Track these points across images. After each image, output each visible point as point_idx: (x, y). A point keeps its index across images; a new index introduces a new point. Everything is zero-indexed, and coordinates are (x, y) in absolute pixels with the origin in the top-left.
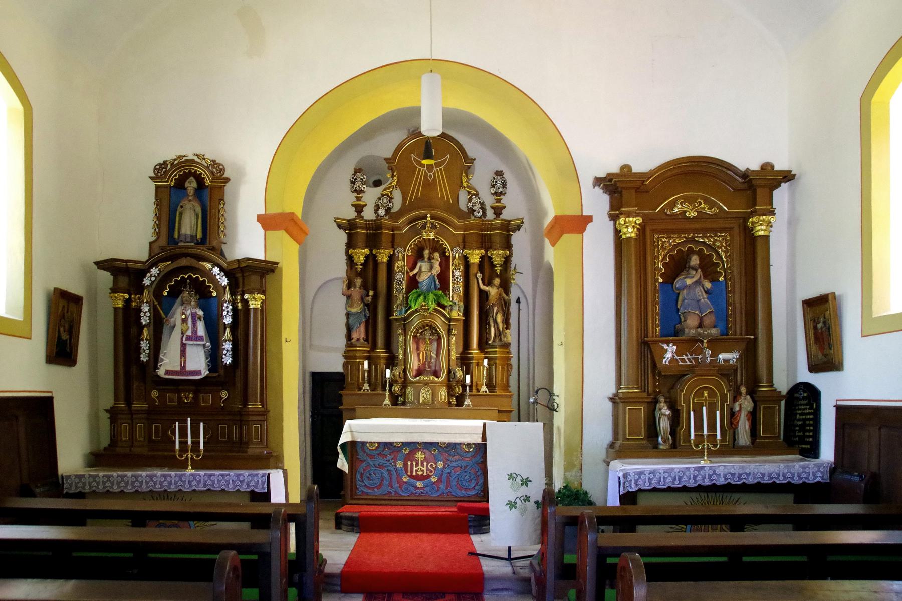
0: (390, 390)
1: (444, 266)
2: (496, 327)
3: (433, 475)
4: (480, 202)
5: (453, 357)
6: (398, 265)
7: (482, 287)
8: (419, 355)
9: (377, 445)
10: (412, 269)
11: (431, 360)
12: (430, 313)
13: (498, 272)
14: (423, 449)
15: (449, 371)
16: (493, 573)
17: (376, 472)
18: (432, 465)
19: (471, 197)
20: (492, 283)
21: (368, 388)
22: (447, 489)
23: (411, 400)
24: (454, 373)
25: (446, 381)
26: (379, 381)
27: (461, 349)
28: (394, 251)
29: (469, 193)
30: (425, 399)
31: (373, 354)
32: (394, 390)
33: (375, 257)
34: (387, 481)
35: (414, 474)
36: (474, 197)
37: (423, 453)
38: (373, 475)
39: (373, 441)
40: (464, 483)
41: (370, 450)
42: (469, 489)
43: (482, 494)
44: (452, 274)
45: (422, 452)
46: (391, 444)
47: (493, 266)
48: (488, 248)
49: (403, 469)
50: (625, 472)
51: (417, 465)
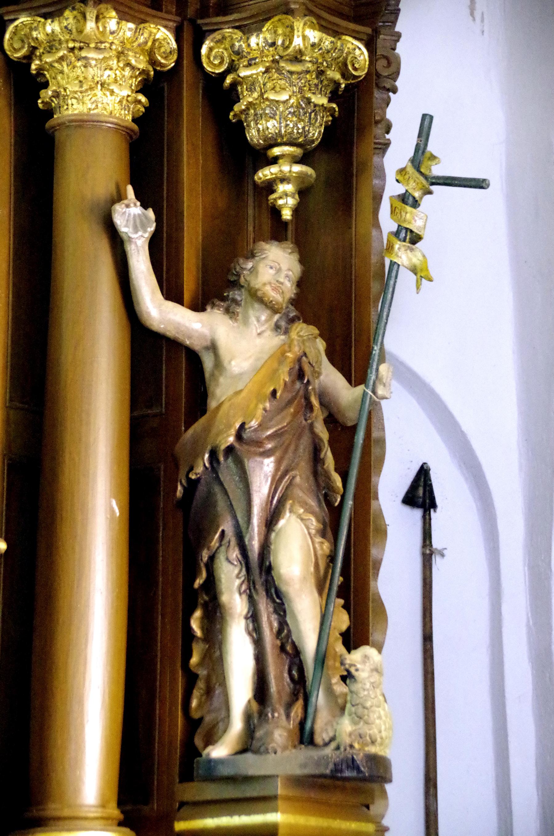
16: (218, 560)
20: (235, 284)
50: (411, 245)
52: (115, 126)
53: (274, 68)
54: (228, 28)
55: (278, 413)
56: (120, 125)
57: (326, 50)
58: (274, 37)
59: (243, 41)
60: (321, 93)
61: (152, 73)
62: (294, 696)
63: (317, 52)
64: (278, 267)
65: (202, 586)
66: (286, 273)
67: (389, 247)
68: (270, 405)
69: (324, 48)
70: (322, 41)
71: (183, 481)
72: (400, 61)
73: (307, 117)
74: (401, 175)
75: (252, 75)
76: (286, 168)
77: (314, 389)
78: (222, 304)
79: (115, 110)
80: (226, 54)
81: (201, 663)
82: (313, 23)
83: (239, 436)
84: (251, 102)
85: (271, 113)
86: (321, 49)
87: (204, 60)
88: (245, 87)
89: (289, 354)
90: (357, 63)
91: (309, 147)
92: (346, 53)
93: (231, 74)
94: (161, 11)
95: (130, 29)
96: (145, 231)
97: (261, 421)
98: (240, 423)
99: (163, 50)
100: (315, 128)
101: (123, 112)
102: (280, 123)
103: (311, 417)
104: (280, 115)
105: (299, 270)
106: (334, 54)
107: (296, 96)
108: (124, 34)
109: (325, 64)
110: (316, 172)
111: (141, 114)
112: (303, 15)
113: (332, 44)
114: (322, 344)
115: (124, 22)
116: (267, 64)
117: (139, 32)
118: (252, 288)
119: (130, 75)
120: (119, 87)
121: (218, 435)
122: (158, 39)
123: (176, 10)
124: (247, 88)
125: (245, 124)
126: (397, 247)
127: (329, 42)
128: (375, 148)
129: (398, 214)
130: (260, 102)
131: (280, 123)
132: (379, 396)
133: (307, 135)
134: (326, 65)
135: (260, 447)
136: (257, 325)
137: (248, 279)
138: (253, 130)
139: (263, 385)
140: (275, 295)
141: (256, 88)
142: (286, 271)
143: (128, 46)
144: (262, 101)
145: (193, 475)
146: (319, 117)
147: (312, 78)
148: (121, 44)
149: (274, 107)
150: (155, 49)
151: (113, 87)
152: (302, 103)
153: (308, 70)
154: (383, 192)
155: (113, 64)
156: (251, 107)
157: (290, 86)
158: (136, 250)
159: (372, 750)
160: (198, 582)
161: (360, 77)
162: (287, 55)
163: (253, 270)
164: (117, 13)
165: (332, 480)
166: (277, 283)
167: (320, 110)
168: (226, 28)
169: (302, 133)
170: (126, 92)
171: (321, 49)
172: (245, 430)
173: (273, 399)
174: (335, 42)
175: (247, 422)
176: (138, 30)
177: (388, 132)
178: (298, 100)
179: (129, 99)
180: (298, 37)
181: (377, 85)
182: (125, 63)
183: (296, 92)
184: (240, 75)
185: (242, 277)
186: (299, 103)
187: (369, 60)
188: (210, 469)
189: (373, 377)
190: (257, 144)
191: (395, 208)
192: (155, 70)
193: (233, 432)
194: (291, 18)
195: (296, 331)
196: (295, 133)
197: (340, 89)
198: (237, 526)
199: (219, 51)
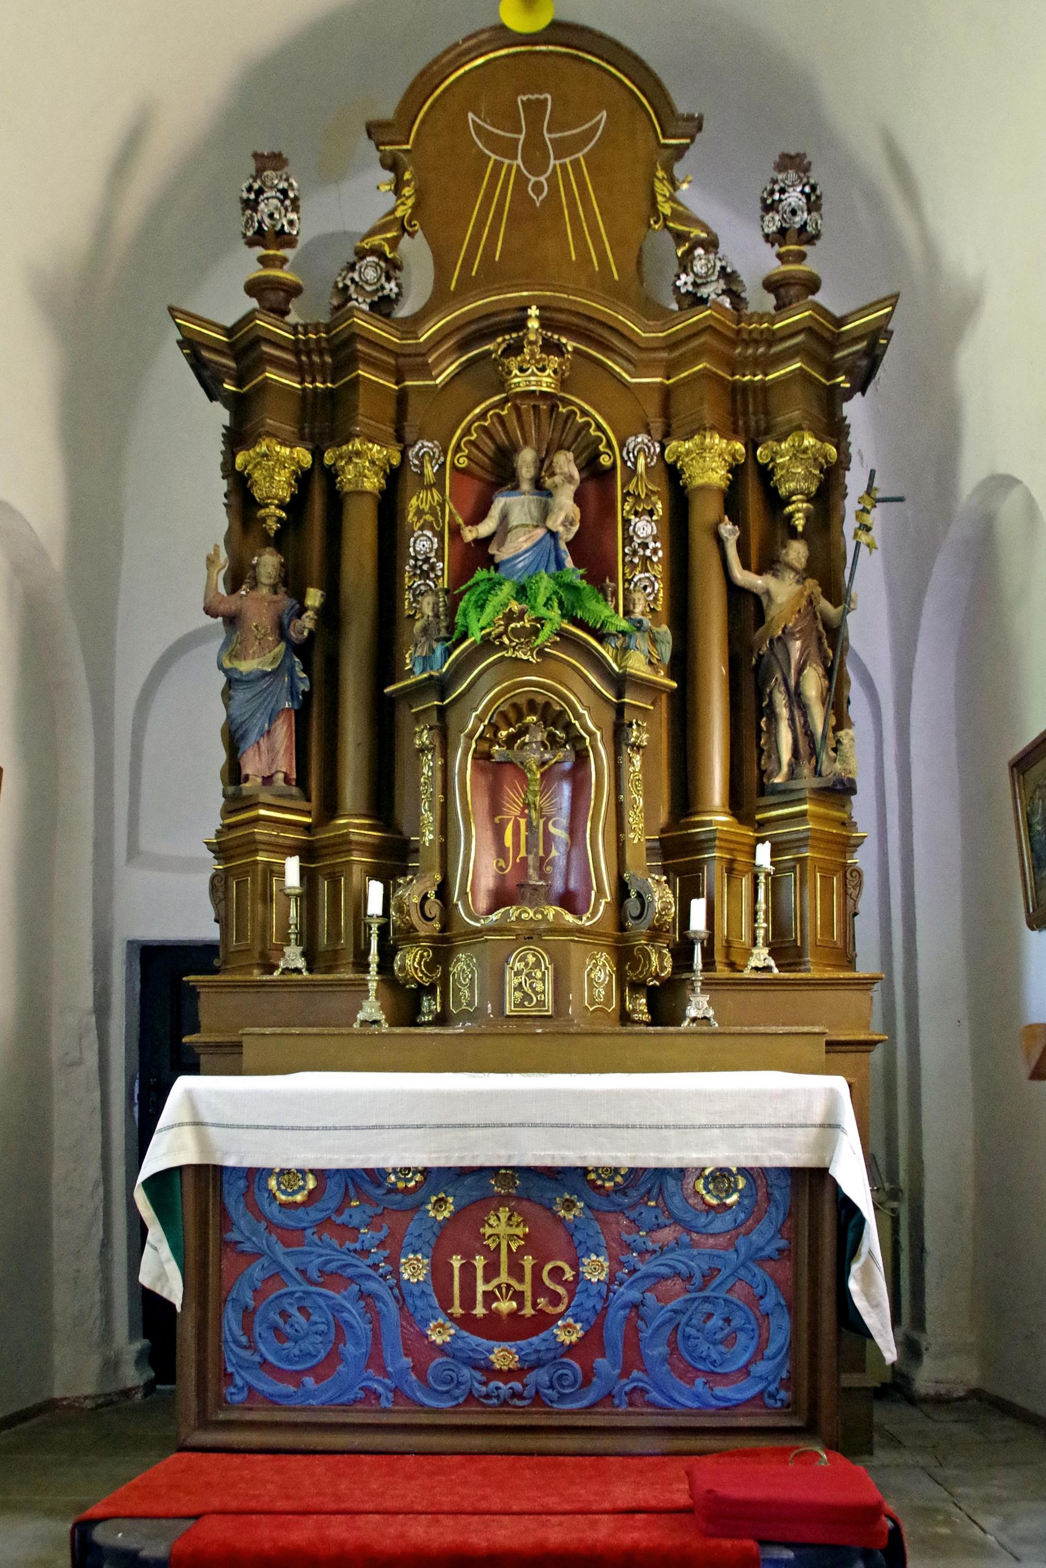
0: (385, 966)
1: (593, 505)
2: (799, 721)
3: (561, 1316)
4: (723, 268)
5: (637, 836)
6: (416, 502)
7: (742, 576)
8: (498, 832)
9: (311, 1184)
10: (479, 516)
11: (547, 851)
12: (541, 653)
13: (800, 523)
14: (518, 1198)
15: (622, 889)
17: (307, 1303)
18: (557, 1273)
19: (690, 252)
20: (778, 561)
21: (301, 963)
22: (625, 1373)
23: (470, 1004)
24: (639, 896)
25: (610, 929)
26: (345, 942)
27: (663, 817)
28: (404, 453)
29: (680, 238)
30: (527, 997)
31: (324, 835)
32: (402, 968)
33: (331, 475)
34: (357, 1344)
35: (479, 1311)
36: (700, 251)
37: (517, 1218)
38: (299, 1318)
39: (292, 1165)
40: (704, 1348)
41: (283, 1205)
42: (725, 1374)
43: (783, 1394)
44: (625, 530)
45: (512, 1210)
46: (376, 1176)
47: (775, 502)
48: (758, 433)
49: (430, 1290)
51: (492, 1271)
62: (811, 755)
65: (767, 706)
81: (765, 744)
83: (783, 632)
147: (811, 461)
159: (851, 776)
160: (764, 704)
170: (723, 472)
198: (783, 674)
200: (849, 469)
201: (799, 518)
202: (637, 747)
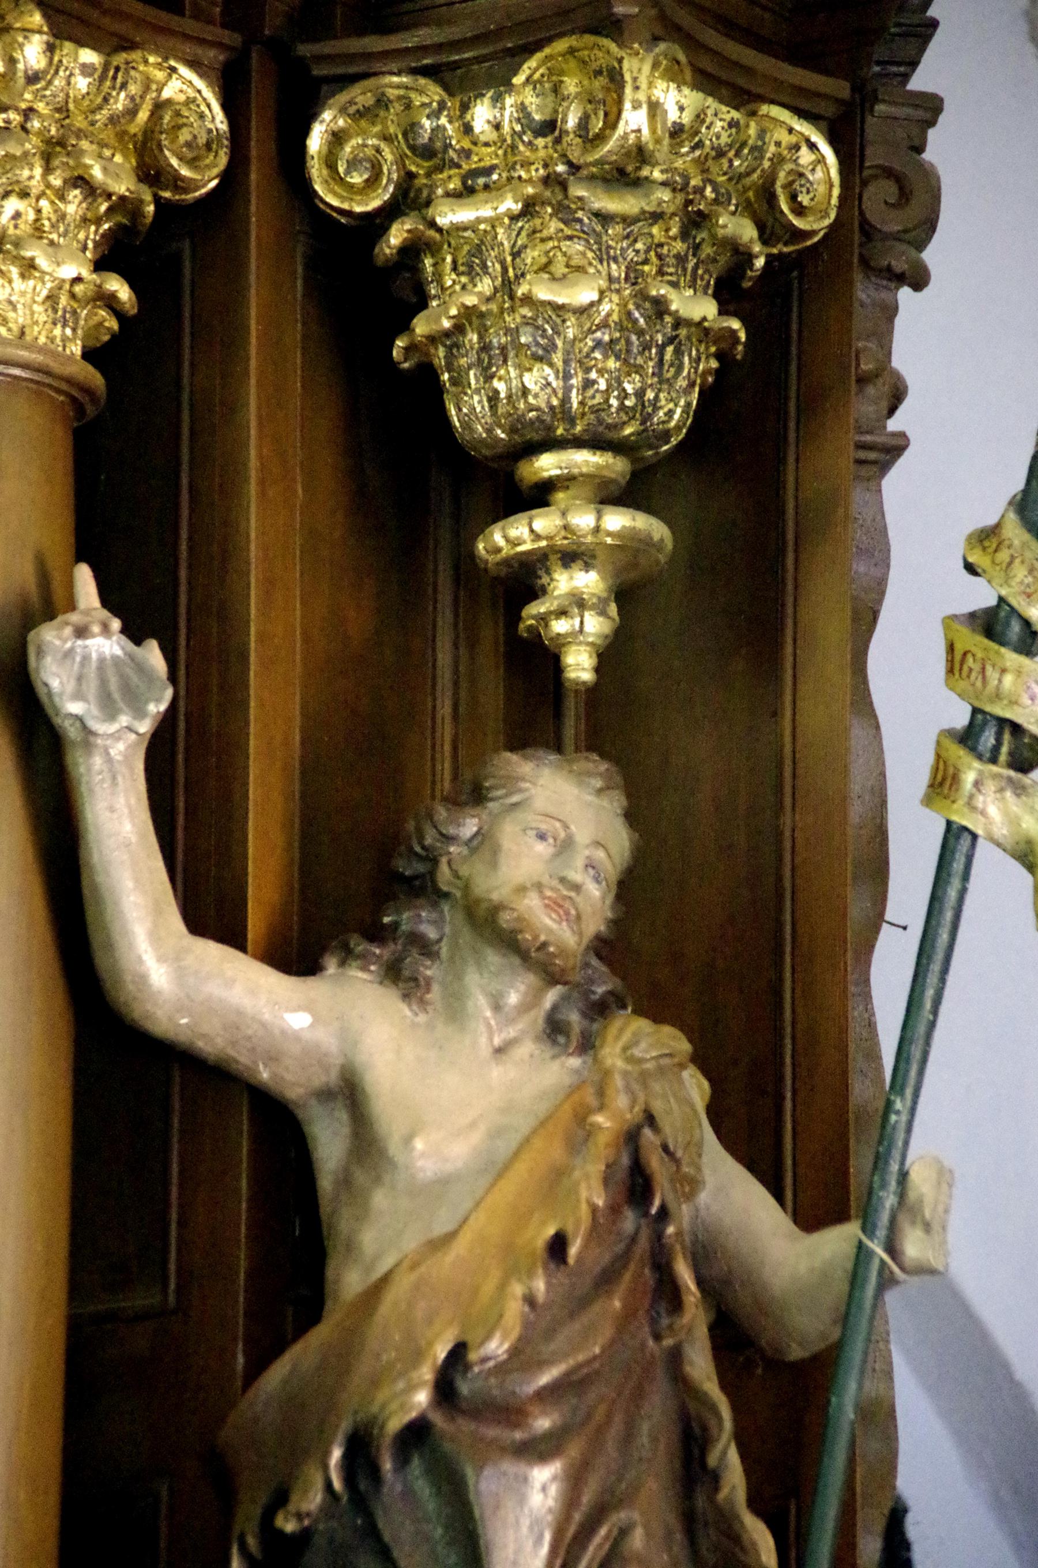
50: (1020, 776)
52: (36, 377)
53: (550, 204)
54: (398, 74)
55: (572, 1315)
56: (48, 373)
57: (713, 148)
58: (551, 105)
59: (448, 116)
60: (693, 285)
61: (151, 208)
63: (688, 153)
64: (562, 835)
66: (587, 853)
67: (944, 779)
68: (549, 1284)
69: (708, 142)
70: (703, 121)
71: (251, 1541)
72: (939, 189)
73: (651, 359)
74: (984, 549)
75: (479, 220)
76: (584, 520)
77: (679, 1234)
78: (378, 951)
79: (36, 323)
80: (388, 155)
82: (678, 62)
84: (474, 306)
85: (538, 344)
86: (699, 145)
87: (316, 171)
88: (449, 259)
89: (599, 1119)
90: (804, 190)
91: (650, 453)
92: (771, 159)
93: (405, 219)
94: (181, 13)
95: (87, 70)
96: (140, 713)
97: (520, 1339)
98: (449, 1346)
99: (184, 136)
100: (674, 395)
101: (57, 331)
102: (567, 377)
103: (675, 1327)
104: (567, 353)
105: (627, 844)
106: (736, 163)
107: (618, 291)
108: (69, 84)
109: (709, 191)
110: (673, 533)
111: (106, 338)
112: (648, 36)
113: (734, 130)
114: (700, 1086)
115: (68, 46)
116: (530, 190)
117: (115, 78)
118: (478, 901)
119: (80, 212)
120: (50, 250)
121: (375, 1383)
122: (169, 102)
123: (223, 14)
124: (454, 262)
125: (446, 376)
126: (969, 778)
127: (726, 125)
128: (860, 462)
129: (974, 675)
130: (502, 311)
131: (567, 377)
132: (908, 1263)
133: (649, 414)
134: (713, 196)
135: (516, 1425)
136: (493, 1022)
137: (464, 871)
138: (476, 398)
139: (520, 1218)
140: (554, 926)
141: (489, 264)
142: (587, 846)
143: (79, 122)
144: (507, 305)
145: (286, 1520)
146: (686, 359)
148: (57, 115)
149: (547, 326)
150: (161, 133)
151: (34, 252)
152: (637, 315)
153: (659, 210)
154: (880, 601)
155: (31, 178)
156: (470, 324)
157: (601, 261)
158: (107, 775)
161: (814, 233)
162: (595, 164)
163: (482, 843)
164: (45, 16)
165: (746, 1543)
166: (560, 887)
167: (689, 338)
168: (392, 73)
169: (633, 408)
171: (699, 145)
172: (467, 1367)
173: (552, 1266)
174: (742, 122)
175: (469, 1338)
176: (111, 73)
177: (892, 411)
178: (623, 305)
179: (79, 289)
180: (637, 105)
181: (865, 263)
182: (67, 174)
183: (618, 279)
184: (440, 221)
185: (444, 869)
186: (629, 314)
187: (841, 181)
188: (345, 1499)
189: (890, 1200)
190: (482, 441)
191: (965, 654)
192: (157, 200)
193: (427, 1373)
194: (613, 47)
195: (620, 1044)
196: (613, 410)
197: (749, 273)
199: (365, 146)
200: (919, 280)
201: (579, 602)
202: (78, 241)
